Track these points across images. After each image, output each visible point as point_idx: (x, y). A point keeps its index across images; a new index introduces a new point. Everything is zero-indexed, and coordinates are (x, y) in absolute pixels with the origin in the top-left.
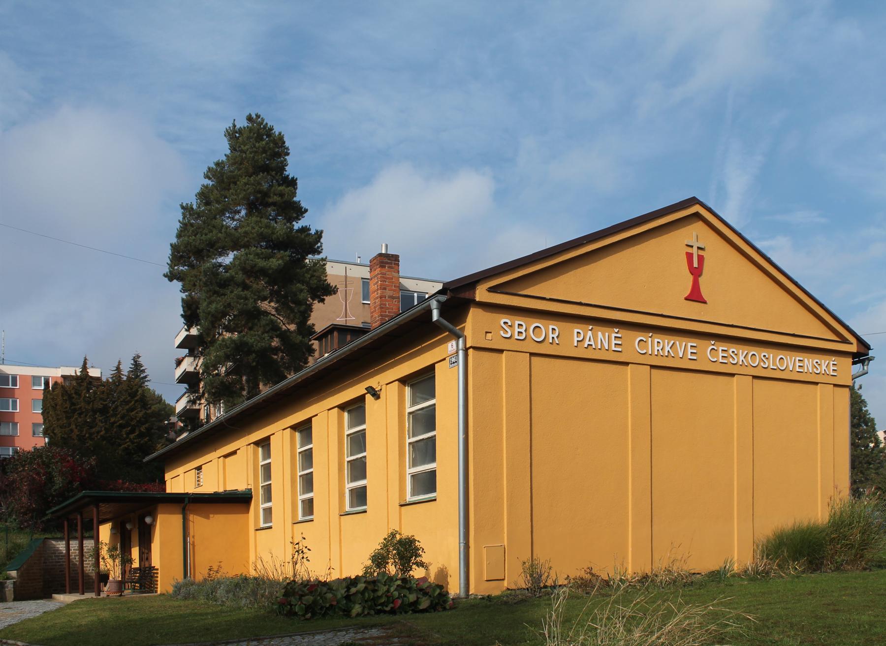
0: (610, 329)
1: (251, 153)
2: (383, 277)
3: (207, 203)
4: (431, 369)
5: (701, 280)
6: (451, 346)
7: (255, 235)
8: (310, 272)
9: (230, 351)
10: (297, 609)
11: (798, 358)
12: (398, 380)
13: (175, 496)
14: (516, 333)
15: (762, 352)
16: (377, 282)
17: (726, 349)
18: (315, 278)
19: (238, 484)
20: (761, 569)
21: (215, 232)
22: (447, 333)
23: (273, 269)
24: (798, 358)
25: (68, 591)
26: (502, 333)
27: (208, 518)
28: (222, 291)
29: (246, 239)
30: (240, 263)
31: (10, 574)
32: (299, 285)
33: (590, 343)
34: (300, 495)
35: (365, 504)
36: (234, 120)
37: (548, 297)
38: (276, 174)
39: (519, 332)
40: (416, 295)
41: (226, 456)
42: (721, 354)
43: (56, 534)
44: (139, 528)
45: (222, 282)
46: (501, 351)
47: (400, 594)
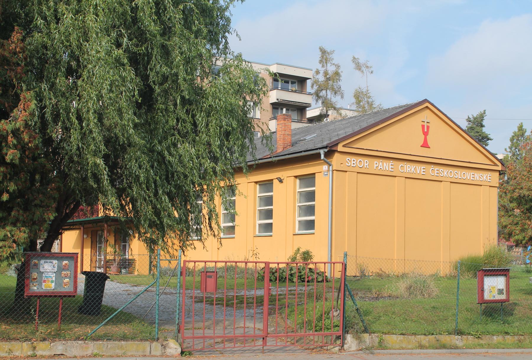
0: (389, 161)
5: (428, 137)
6: (325, 167)
11: (472, 173)
15: (456, 170)
16: (282, 127)
20: (453, 274)
24: (472, 173)
42: (436, 172)
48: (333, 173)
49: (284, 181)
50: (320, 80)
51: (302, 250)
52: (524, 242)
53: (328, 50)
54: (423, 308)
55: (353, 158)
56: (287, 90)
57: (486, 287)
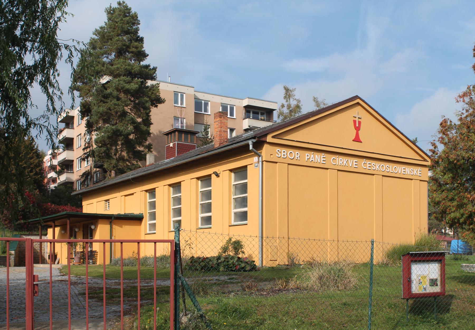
1: (120, 23)
2: (221, 122)
3: (94, 48)
4: (246, 167)
5: (359, 132)
6: (255, 159)
7: (123, 69)
8: (151, 91)
9: (110, 134)
10: (198, 268)
11: (403, 168)
12: (229, 170)
13: (107, 216)
14: (283, 155)
16: (218, 124)
17: (370, 163)
18: (153, 94)
19: (136, 211)
20: (385, 262)
21: (100, 66)
22: (254, 153)
23: (133, 89)
24: (403, 168)
25: (40, 262)
26: (277, 155)
27: (122, 227)
28: (105, 100)
29: (118, 72)
30: (116, 85)
31: (11, 252)
32: (145, 98)
33: (312, 160)
34: (172, 218)
35: (211, 224)
36: (111, 4)
37: (296, 140)
38: (134, 36)
39: (284, 155)
40: (203, 102)
41: (126, 196)
42: (368, 165)
43: (25, 232)
44: (83, 231)
45: (106, 95)
46: (276, 163)
47: (238, 263)
48: (262, 164)
49: (221, 175)
50: (284, 112)
51: (233, 240)
52: (462, 220)
53: (291, 88)
54: (331, 304)
55: (283, 150)
56: (257, 119)
57: (414, 277)
